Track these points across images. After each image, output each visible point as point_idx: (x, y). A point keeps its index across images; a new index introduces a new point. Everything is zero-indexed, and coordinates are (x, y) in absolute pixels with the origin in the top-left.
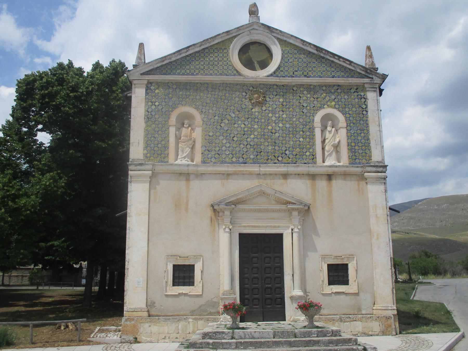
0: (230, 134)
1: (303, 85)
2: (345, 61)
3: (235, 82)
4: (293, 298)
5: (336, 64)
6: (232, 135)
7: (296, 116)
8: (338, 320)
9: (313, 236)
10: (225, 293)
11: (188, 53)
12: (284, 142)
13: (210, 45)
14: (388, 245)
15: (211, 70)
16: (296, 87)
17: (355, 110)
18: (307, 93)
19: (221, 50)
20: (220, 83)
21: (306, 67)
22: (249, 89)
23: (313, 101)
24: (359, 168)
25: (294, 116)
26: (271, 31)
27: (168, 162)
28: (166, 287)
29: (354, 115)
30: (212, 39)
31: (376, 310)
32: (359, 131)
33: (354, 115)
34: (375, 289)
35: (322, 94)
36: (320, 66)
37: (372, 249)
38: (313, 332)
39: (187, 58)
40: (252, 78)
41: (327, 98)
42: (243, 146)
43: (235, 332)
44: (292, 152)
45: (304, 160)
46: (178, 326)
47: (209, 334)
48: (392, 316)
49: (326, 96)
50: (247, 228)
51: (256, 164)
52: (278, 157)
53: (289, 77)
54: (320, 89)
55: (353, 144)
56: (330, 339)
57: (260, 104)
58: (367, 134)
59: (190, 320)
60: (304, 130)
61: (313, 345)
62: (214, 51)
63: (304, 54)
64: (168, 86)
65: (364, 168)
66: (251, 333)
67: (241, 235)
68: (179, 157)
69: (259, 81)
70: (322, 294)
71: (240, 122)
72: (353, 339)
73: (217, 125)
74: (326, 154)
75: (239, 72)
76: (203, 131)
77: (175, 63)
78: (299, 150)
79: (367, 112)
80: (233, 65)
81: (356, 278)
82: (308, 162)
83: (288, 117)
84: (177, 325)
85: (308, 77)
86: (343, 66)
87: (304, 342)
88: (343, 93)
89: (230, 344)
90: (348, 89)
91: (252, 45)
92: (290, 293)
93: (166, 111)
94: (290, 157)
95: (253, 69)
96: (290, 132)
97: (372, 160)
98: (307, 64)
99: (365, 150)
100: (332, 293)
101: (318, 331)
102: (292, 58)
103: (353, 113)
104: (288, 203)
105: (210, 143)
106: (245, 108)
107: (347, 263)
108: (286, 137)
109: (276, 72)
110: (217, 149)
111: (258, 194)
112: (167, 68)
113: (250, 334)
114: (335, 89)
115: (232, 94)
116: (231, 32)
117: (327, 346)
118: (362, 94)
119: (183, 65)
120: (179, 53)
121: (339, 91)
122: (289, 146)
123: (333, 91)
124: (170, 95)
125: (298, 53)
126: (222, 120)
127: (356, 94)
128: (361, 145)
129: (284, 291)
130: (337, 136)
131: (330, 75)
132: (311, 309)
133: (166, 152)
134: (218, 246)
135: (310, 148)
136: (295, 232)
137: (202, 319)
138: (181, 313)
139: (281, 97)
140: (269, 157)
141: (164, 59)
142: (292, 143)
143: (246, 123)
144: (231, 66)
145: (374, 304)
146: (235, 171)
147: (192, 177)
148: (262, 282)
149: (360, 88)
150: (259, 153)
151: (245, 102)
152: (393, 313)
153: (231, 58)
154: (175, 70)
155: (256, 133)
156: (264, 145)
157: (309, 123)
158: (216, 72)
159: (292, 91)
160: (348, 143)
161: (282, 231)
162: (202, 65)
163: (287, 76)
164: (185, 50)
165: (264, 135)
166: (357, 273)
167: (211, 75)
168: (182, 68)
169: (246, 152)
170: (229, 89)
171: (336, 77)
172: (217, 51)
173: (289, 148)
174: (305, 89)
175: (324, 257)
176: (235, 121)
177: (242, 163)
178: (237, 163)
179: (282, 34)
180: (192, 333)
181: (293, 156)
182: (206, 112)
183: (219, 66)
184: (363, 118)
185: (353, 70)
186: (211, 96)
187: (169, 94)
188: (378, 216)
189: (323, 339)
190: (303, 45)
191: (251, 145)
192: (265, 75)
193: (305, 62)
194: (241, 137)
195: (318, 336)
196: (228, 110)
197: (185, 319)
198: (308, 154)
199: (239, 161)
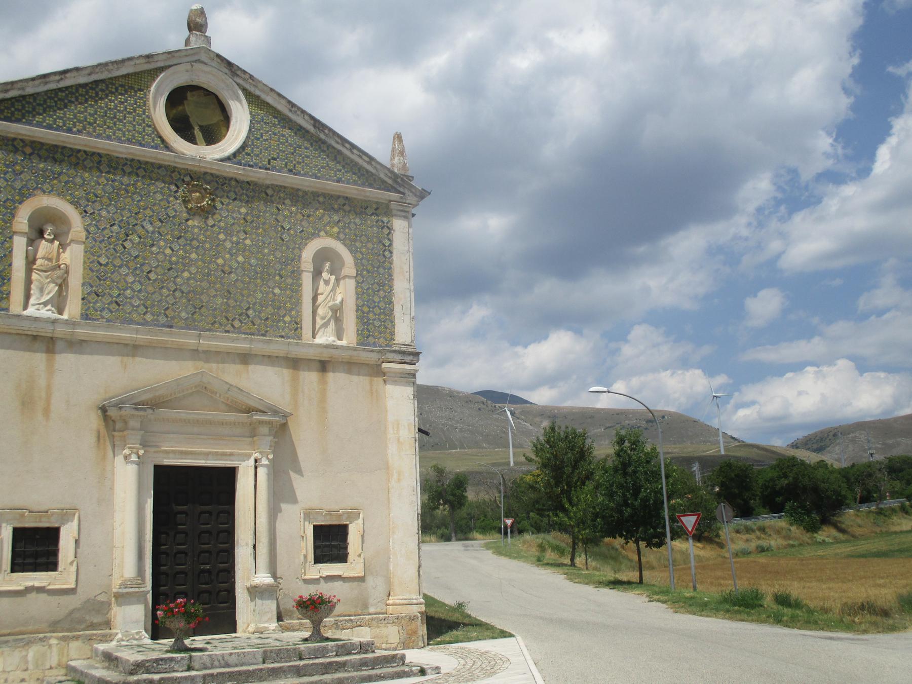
0: (142, 265)
1: (285, 187)
2: (361, 154)
3: (157, 162)
4: (257, 589)
5: (345, 157)
6: (146, 268)
7: (269, 244)
8: (332, 626)
9: (292, 473)
10: (129, 583)
11: (62, 84)
12: (245, 292)
13: (110, 76)
14: (415, 492)
15: (109, 128)
16: (272, 188)
17: (372, 246)
18: (290, 203)
19: (133, 91)
20: (126, 159)
21: (293, 154)
22: (183, 180)
23: (301, 221)
24: (375, 353)
25: (265, 244)
26: (232, 72)
27: (7, 309)
28: (901, 551)
29: (370, 256)
30: (115, 66)
31: (393, 605)
32: (376, 285)
33: (370, 256)
34: (391, 569)
35: (317, 209)
36: (317, 157)
37: (389, 499)
38: (330, 648)
39: (60, 94)
40: (192, 159)
41: (326, 219)
42: (168, 293)
43: (195, 656)
44: (259, 312)
45: (281, 331)
46: (27, 655)
47: (145, 664)
48: (419, 615)
49: (323, 215)
50: (171, 455)
51: (190, 330)
52: (233, 320)
53: (260, 168)
54: (314, 200)
55: (366, 309)
56: (363, 658)
57: (205, 213)
58: (389, 293)
59: (53, 642)
60: (283, 272)
61: (336, 670)
62: (117, 89)
63: (290, 129)
64: (13, 145)
65: (383, 353)
66: (223, 658)
67: (157, 468)
68: (32, 300)
69: (205, 168)
70: (304, 580)
71: (162, 243)
72: (398, 656)
73: (117, 244)
74: (319, 322)
75: (167, 143)
76: (86, 252)
77: (31, 100)
78: (272, 311)
79: (391, 253)
80: (154, 125)
81: (75, 557)
82: (287, 334)
83: (255, 245)
84: (24, 653)
85: (295, 174)
86: (356, 164)
87: (320, 667)
88: (353, 212)
89: (193, 679)
90: (362, 208)
91: (191, 91)
92: (249, 579)
93: (8, 199)
94: (255, 322)
95: (192, 140)
96: (258, 274)
97: (394, 340)
98: (295, 148)
99: (384, 322)
100: (321, 577)
101: (338, 646)
102: (268, 132)
103: (369, 252)
104: (249, 410)
105: (100, 280)
106: (173, 217)
107: (348, 523)
108: (250, 282)
109: (237, 155)
110: (116, 292)
111: (194, 390)
112: (14, 107)
113: (220, 658)
114: (339, 205)
115: (148, 185)
116: (156, 58)
117: (358, 671)
118: (385, 219)
119: (50, 107)
120: (43, 80)
121: (347, 208)
122: (254, 301)
123: (336, 206)
124: (18, 167)
125: (279, 125)
126: (127, 236)
127: (374, 217)
128: (379, 311)
129: (234, 577)
130: (338, 290)
131: (333, 177)
132: (323, 607)
133: (5, 288)
134: (112, 489)
135: (292, 309)
136: (262, 466)
137: (77, 638)
138: (30, 627)
139: (244, 204)
140: (216, 318)
141: (9, 87)
142: (259, 295)
143: (176, 247)
144: (150, 126)
145: (389, 595)
146: (64, 332)
147: (59, 345)
148: (193, 561)
149: (382, 210)
150: (197, 310)
151: (174, 205)
152: (419, 610)
153: (152, 111)
154: (31, 115)
155: (193, 270)
156: (208, 295)
157: (292, 261)
158: (119, 134)
159: (263, 195)
160: (357, 306)
161: (237, 462)
162: (90, 115)
163: (256, 165)
164: (58, 78)
165: (209, 274)
166: (363, 542)
167: (108, 138)
168: (47, 113)
169: (173, 305)
170: (144, 173)
171: (343, 182)
172: (123, 92)
173: (254, 304)
174: (288, 196)
175: (308, 514)
176: (153, 240)
177: (164, 326)
178: (155, 325)
179: (254, 83)
180: (56, 668)
181: (261, 320)
182: (94, 213)
183: (125, 123)
184: (384, 262)
185: (372, 174)
186: (106, 182)
187: (14, 164)
188: (401, 440)
189: (351, 659)
190: (291, 111)
191: (183, 292)
192: (217, 156)
193: (291, 145)
194: (164, 274)
195: (338, 654)
196: (140, 216)
197: (41, 639)
198: (287, 319)
199: (157, 320)
